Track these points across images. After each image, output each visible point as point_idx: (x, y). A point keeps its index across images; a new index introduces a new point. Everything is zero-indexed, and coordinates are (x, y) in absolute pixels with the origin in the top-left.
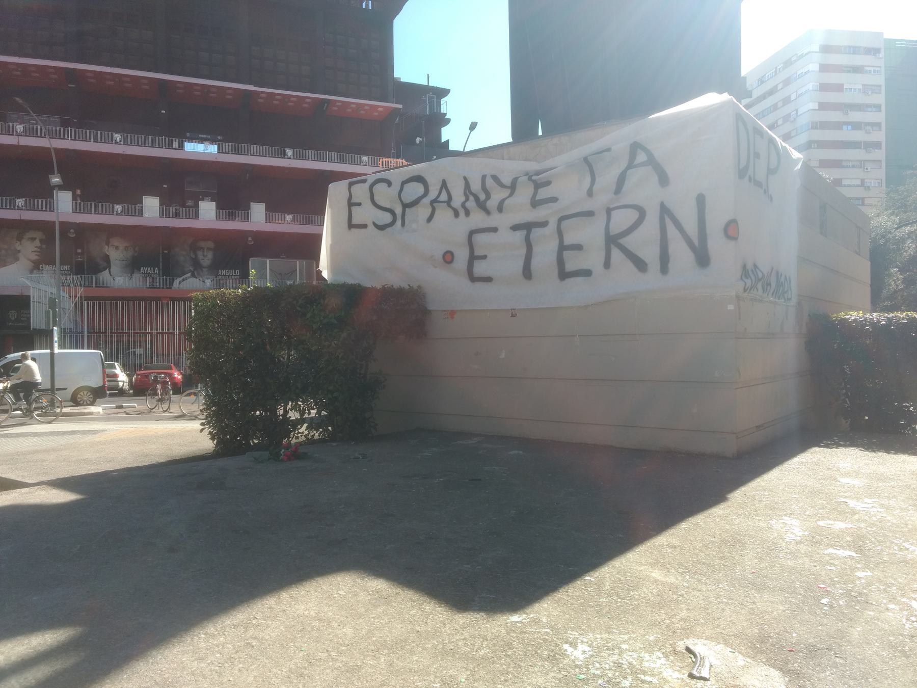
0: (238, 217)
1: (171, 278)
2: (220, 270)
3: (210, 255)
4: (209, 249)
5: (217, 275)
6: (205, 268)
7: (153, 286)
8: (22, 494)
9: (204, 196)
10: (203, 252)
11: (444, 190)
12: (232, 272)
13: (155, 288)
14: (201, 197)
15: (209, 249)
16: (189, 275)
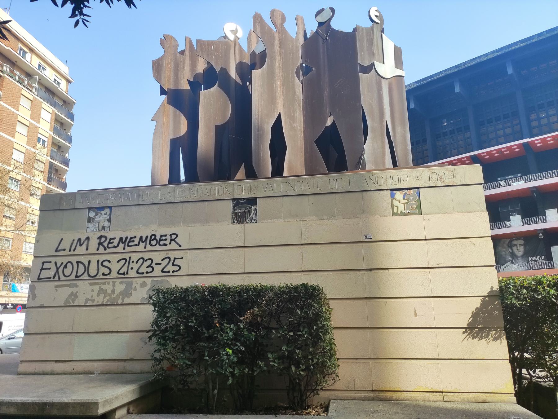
0: (539, 221)
1: (499, 266)
2: (530, 258)
3: (522, 249)
4: (520, 245)
5: (528, 261)
6: (519, 257)
7: (542, 267)
8: (297, 417)
9: (513, 212)
10: (517, 247)
11: (58, 267)
12: (539, 258)
13: (541, 269)
14: (510, 214)
15: (520, 245)
16: (510, 262)
